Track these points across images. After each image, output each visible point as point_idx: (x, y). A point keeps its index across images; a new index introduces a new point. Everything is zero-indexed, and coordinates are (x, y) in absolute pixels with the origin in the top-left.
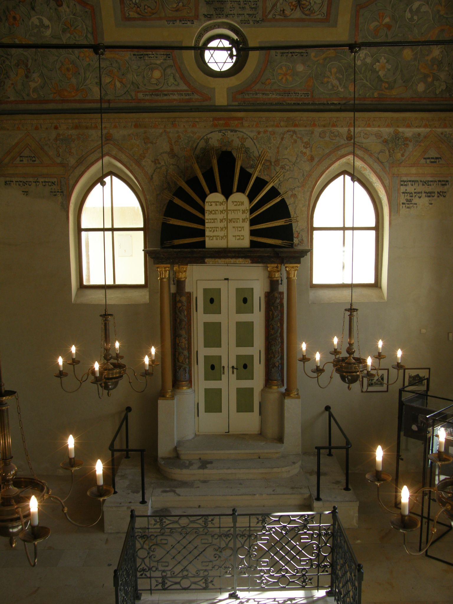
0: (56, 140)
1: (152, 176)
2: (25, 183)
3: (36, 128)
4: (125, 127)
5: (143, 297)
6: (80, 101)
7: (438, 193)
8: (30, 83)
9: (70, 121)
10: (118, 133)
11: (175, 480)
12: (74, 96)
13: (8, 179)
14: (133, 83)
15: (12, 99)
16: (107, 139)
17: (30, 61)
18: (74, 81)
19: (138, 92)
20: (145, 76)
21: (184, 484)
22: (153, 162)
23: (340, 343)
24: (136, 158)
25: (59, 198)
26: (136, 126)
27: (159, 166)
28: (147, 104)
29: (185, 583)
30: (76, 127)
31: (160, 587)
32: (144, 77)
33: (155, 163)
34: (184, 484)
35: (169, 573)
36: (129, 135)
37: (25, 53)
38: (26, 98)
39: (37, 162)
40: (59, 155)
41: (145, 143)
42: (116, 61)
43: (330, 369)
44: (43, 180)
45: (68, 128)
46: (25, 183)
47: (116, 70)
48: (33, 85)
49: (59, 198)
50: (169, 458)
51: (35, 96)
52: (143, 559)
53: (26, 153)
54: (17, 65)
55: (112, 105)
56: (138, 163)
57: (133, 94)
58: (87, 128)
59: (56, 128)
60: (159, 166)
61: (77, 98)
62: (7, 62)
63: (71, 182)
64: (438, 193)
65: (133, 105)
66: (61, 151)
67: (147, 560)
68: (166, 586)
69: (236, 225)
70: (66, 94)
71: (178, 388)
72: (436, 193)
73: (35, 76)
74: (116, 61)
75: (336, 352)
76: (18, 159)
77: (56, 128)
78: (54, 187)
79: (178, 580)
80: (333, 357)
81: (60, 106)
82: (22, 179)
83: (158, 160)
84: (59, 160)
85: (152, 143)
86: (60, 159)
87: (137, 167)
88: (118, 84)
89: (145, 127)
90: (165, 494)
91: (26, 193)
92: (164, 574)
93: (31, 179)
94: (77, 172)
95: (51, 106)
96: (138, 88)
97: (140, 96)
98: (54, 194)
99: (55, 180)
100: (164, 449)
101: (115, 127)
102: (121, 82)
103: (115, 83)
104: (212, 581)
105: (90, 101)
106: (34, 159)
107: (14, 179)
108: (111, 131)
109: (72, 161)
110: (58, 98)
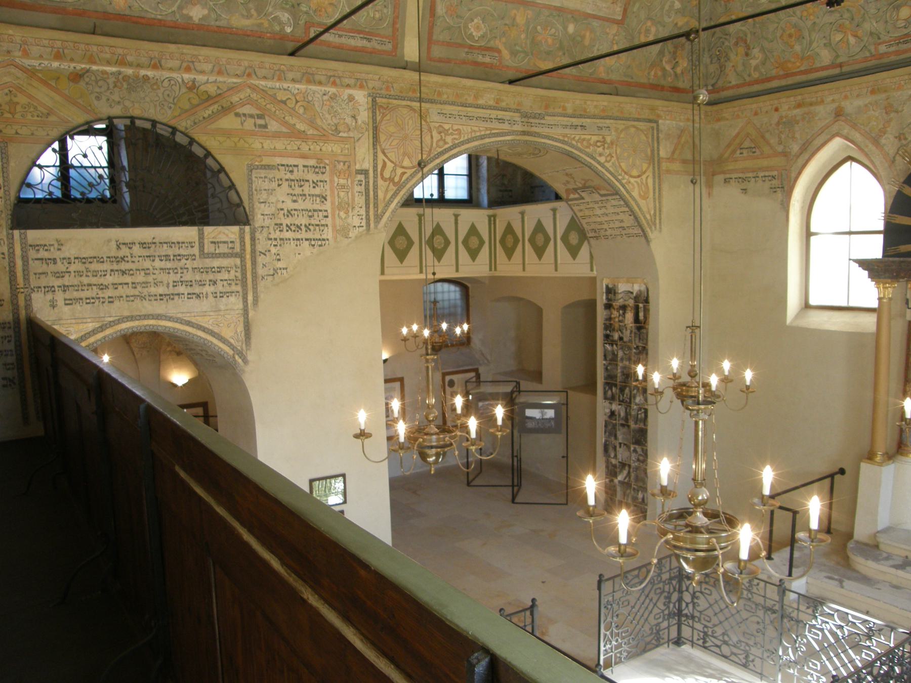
0: (778, 124)
1: (894, 157)
2: (744, 180)
3: (756, 114)
4: (858, 96)
5: (869, 322)
6: (806, 72)
7: (287, 225)
8: (751, 61)
9: (792, 99)
10: (850, 106)
11: (858, 572)
12: (799, 67)
13: (728, 176)
14: (871, 34)
15: (734, 83)
16: (839, 114)
17: (749, 36)
18: (798, 48)
19: (879, 44)
20: (888, 19)
21: (865, 580)
22: (896, 137)
23: (681, 367)
24: (873, 135)
25: (779, 195)
26: (873, 92)
27: (904, 142)
28: (893, 58)
29: (726, 650)
30: (799, 106)
31: (701, 642)
32: (886, 22)
33: (900, 139)
34: (865, 580)
35: (710, 630)
36: (866, 106)
37: (743, 28)
38: (748, 79)
39: (758, 153)
40: (780, 143)
41: (886, 113)
42: (848, 10)
43: (669, 394)
44: (762, 174)
45: (789, 108)
46: (744, 180)
47: (848, 22)
48: (754, 63)
49: (779, 195)
50: (866, 545)
51: (756, 75)
52: (687, 604)
53: (747, 144)
54: (736, 44)
55: (846, 69)
56: (876, 142)
57: (872, 48)
58: (811, 104)
59: (777, 110)
60: (904, 142)
61: (802, 68)
62: (727, 43)
63: (793, 175)
64: (287, 225)
65: (874, 62)
66: (783, 136)
67: (690, 606)
68: (707, 645)
69: (43, 254)
70: (790, 65)
71: (902, 454)
72: (284, 225)
73: (756, 52)
74: (848, 10)
75: (675, 377)
76: (738, 152)
77: (777, 110)
78: (774, 182)
79: (719, 643)
80: (671, 383)
81: (783, 82)
82: (741, 175)
83: (903, 134)
84: (780, 149)
85: (897, 112)
86: (782, 147)
87: (874, 148)
88: (852, 40)
89: (885, 91)
90: (827, 580)
91: (745, 191)
92: (706, 630)
93: (750, 175)
94: (800, 162)
95: (775, 84)
96: (879, 38)
97: (883, 49)
98: (774, 190)
99: (775, 173)
100: (861, 532)
101: (846, 97)
102: (855, 36)
103: (848, 40)
104: (753, 661)
105: (817, 70)
106: (261, 122)
107: (734, 176)
108: (843, 104)
109: (795, 148)
110: (781, 73)
